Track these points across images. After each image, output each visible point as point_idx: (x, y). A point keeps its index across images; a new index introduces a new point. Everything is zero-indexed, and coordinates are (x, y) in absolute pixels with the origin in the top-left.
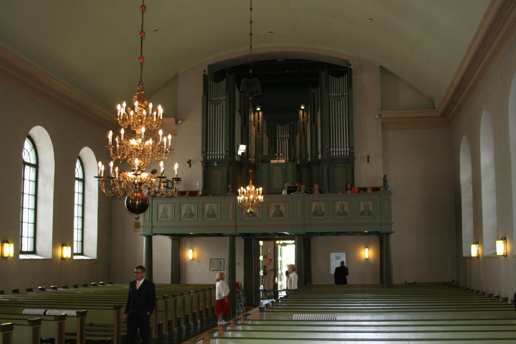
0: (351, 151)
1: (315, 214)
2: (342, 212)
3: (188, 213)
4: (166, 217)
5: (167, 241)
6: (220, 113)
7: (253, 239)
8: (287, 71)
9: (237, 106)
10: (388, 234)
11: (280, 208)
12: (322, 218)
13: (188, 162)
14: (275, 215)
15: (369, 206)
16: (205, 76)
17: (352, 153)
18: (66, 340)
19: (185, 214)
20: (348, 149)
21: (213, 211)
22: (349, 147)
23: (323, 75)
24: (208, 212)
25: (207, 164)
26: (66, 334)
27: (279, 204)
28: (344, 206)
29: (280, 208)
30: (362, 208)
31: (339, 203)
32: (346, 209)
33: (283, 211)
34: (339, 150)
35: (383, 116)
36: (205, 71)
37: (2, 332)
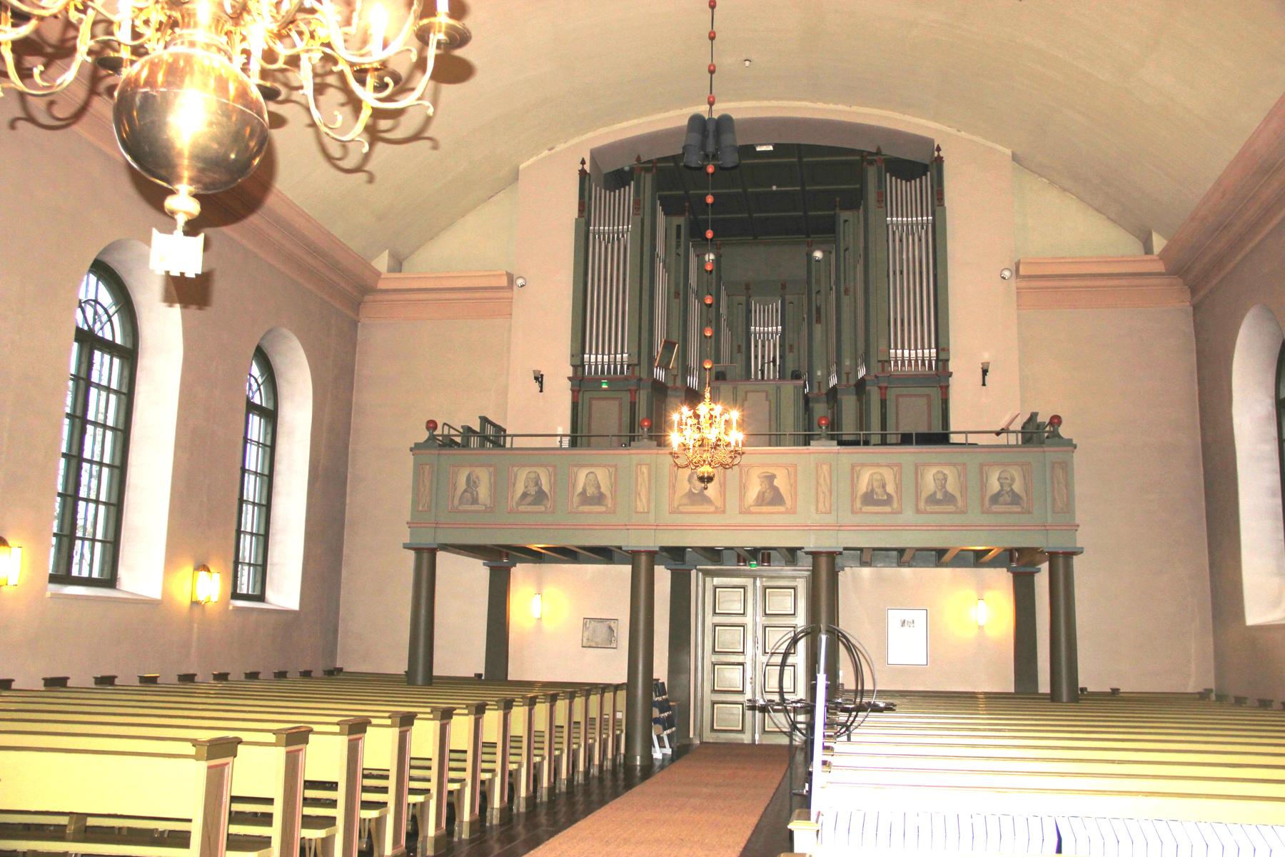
0: (942, 356)
1: (869, 499)
2: (939, 496)
3: (532, 490)
4: (475, 501)
5: (477, 572)
6: (616, 268)
7: (693, 573)
8: (774, 188)
9: (660, 250)
10: (1069, 555)
11: (776, 483)
12: (887, 509)
13: (536, 378)
14: (761, 500)
15: (1013, 480)
16: (583, 173)
17: (943, 361)
18: (305, 799)
19: (525, 495)
20: (934, 351)
21: (599, 487)
22: (937, 347)
23: (872, 172)
24: (584, 492)
25: (581, 383)
26: (452, 751)
27: (772, 471)
28: (945, 479)
29: (776, 483)
30: (994, 486)
31: (933, 470)
32: (951, 486)
33: (782, 491)
34: (909, 354)
35: (1022, 272)
36: (583, 162)
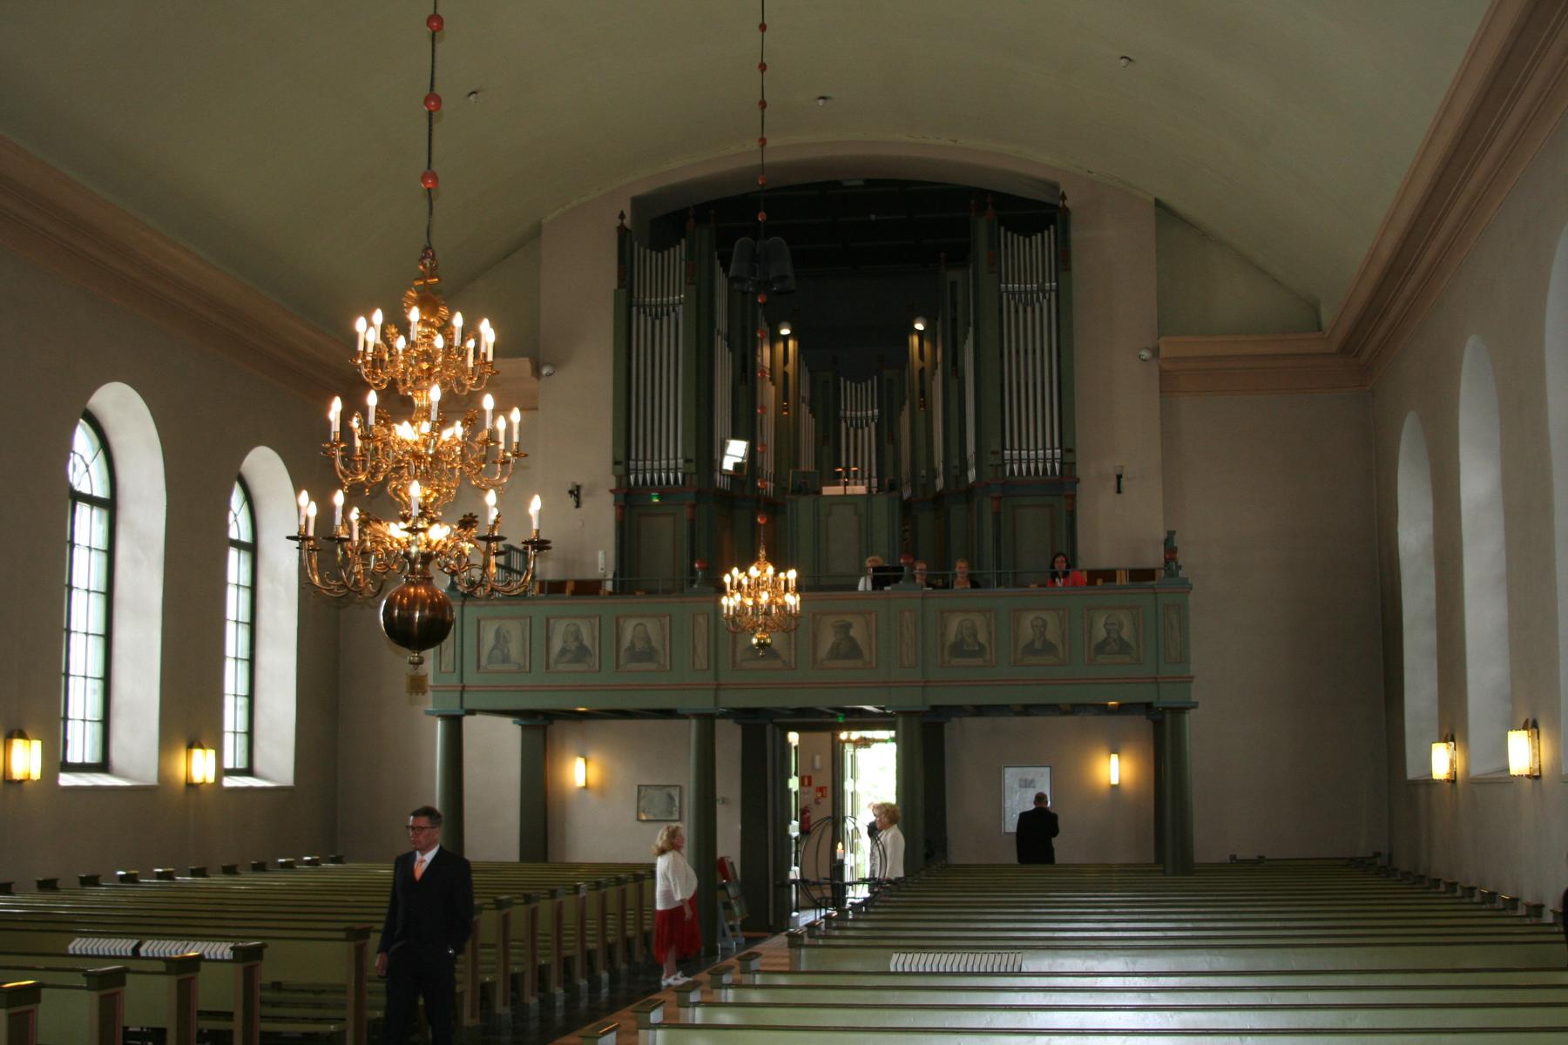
0: (1068, 458)
1: (958, 649)
2: (1038, 645)
3: (573, 646)
4: (506, 659)
5: (508, 733)
6: (670, 343)
7: (769, 727)
8: (873, 217)
9: (722, 323)
10: (1179, 711)
11: (852, 633)
12: (978, 661)
13: (571, 492)
14: (835, 653)
15: (1121, 625)
16: (622, 231)
17: (1068, 466)
18: (200, 1033)
19: (563, 651)
20: (1058, 451)
21: (648, 640)
22: (1061, 447)
23: (982, 226)
24: (633, 645)
25: (629, 500)
26: (200, 1013)
27: (848, 619)
28: (1045, 625)
29: (852, 633)
30: (1101, 633)
31: (1031, 616)
32: (1052, 634)
33: (859, 642)
34: (1031, 455)
35: (1163, 353)
36: (622, 216)
37: (7, 1007)
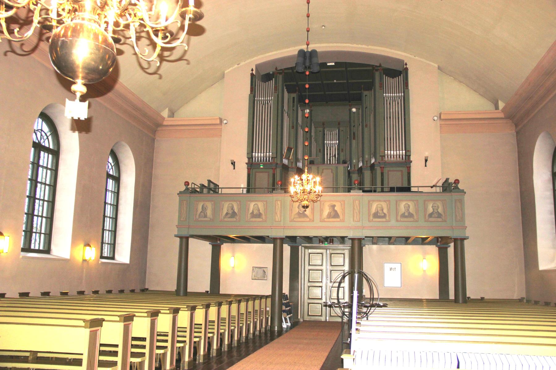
0: (408, 154)
1: (376, 215)
2: (406, 214)
3: (230, 212)
4: (206, 216)
5: (206, 247)
6: (267, 116)
7: (300, 247)
8: (335, 81)
9: (286, 108)
10: (462, 240)
11: (336, 208)
12: (384, 220)
13: (232, 163)
14: (329, 216)
15: (438, 207)
16: (252, 75)
17: (408, 156)
19: (227, 214)
20: (404, 152)
21: (259, 210)
22: (405, 150)
23: (377, 74)
24: (253, 212)
25: (252, 165)
27: (334, 203)
28: (409, 207)
29: (336, 208)
30: (430, 210)
31: (404, 203)
32: (412, 210)
33: (338, 212)
34: (393, 153)
35: (442, 117)
36: (252, 70)
37: (124, 322)
